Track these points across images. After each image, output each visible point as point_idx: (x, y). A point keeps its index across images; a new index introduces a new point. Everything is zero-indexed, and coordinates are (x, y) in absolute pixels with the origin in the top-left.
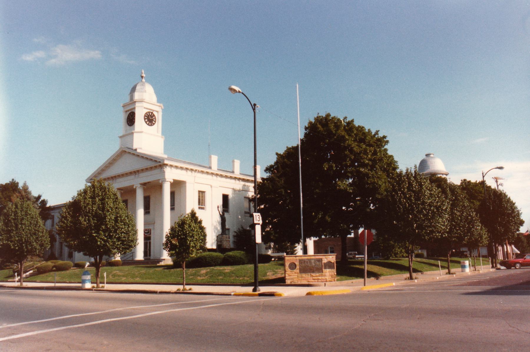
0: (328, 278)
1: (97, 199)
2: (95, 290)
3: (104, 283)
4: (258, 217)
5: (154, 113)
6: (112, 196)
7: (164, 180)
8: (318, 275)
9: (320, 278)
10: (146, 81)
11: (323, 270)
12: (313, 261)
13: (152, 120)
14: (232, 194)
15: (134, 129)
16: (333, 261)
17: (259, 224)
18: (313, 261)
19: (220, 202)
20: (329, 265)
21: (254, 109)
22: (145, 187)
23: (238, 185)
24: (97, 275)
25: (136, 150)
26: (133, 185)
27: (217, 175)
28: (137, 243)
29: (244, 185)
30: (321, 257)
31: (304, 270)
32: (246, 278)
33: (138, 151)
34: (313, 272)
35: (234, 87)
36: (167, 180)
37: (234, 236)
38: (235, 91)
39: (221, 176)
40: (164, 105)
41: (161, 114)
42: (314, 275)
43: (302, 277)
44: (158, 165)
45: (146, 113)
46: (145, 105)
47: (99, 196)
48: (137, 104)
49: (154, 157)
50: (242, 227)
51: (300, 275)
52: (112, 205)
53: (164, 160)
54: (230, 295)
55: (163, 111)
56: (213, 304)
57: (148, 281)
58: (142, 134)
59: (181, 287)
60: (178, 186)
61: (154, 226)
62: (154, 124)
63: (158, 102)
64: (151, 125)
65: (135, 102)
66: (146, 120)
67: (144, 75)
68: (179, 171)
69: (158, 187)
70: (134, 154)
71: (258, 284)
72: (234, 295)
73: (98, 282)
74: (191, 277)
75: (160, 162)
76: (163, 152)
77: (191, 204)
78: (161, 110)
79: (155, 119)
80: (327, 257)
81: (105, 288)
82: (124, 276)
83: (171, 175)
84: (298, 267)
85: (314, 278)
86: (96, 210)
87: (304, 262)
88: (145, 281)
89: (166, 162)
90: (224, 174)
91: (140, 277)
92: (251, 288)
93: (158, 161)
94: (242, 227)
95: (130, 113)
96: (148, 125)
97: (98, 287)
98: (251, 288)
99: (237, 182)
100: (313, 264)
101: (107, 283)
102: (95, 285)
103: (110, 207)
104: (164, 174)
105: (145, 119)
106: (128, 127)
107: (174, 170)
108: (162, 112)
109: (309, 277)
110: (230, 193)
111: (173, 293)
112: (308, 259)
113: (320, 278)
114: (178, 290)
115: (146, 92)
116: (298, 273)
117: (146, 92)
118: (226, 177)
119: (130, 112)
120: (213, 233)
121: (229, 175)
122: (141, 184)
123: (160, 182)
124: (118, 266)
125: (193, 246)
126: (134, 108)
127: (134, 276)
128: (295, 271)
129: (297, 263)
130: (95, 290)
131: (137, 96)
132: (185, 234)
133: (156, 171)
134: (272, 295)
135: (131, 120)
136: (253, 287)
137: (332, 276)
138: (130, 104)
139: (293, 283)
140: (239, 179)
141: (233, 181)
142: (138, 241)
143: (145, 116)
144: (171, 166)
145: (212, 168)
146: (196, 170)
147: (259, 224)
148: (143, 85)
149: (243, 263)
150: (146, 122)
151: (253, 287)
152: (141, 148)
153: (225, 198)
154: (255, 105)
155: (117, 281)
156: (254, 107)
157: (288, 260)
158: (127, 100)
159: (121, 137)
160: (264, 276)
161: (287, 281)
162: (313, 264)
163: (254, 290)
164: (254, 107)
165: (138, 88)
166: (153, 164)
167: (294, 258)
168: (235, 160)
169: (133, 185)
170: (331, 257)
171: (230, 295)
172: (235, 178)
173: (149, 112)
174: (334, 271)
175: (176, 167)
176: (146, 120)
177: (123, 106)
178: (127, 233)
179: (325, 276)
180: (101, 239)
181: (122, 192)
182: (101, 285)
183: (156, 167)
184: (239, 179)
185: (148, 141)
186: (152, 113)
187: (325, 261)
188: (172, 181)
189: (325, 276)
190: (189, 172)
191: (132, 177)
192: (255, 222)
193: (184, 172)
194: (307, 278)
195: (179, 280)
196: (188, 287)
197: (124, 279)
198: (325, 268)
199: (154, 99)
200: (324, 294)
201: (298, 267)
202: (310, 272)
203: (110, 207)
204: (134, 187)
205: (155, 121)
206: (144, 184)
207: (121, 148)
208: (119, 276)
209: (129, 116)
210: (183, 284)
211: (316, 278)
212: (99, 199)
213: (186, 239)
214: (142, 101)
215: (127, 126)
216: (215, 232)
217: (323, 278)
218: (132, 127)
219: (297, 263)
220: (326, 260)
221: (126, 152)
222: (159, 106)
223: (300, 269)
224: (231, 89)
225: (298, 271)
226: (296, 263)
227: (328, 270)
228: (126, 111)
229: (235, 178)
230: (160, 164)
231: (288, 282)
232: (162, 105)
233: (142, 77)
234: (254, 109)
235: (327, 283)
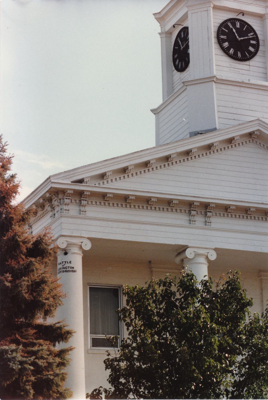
45: (224, 24)
62: (253, 55)
96: (234, 57)
105: (220, 42)
150: (226, 51)
173: (233, 21)
228: (169, 33)
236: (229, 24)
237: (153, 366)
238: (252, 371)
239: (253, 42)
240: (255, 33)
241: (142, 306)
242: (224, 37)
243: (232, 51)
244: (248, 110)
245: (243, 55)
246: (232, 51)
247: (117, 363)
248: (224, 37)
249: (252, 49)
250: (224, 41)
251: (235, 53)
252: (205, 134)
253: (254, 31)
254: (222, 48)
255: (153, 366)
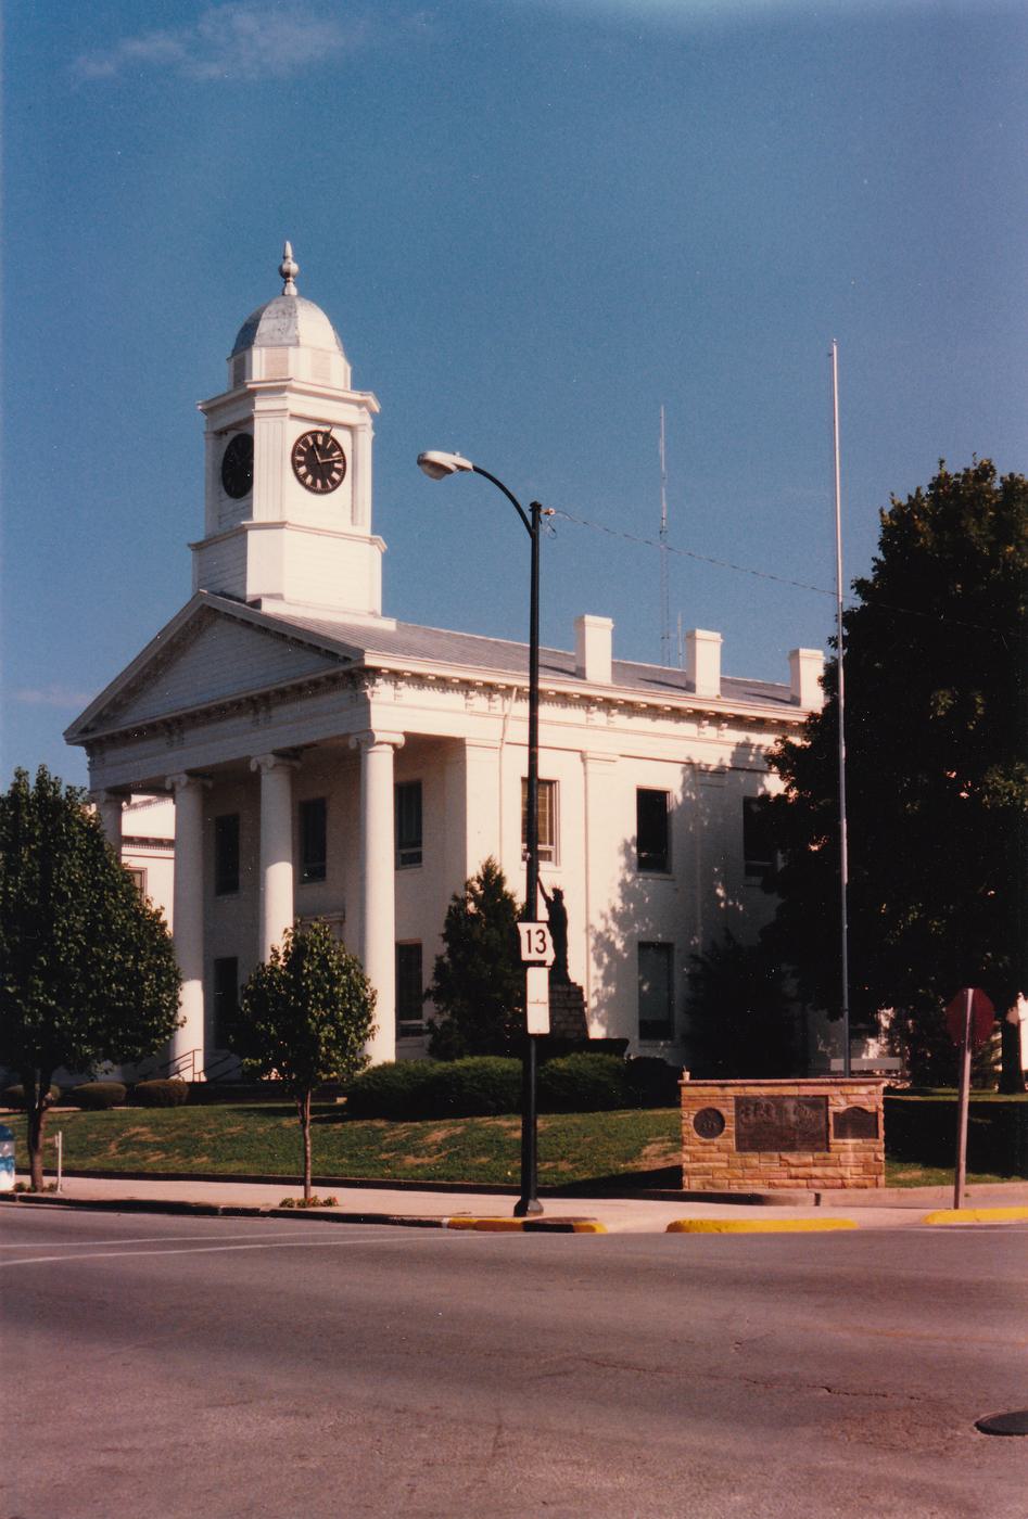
0: (850, 1172)
1: (25, 852)
2: (23, 1199)
3: (54, 1173)
4: (536, 939)
5: (337, 434)
6: (81, 841)
7: (367, 739)
8: (809, 1159)
9: (817, 1171)
10: (301, 294)
11: (832, 1140)
12: (790, 1105)
13: (330, 467)
14: (685, 787)
15: (249, 514)
16: (870, 1108)
17: (541, 964)
18: (790, 1105)
19: (626, 825)
20: (856, 1123)
21: (533, 531)
22: (297, 764)
23: (716, 748)
24: (33, 1146)
25: (257, 604)
26: (249, 758)
27: (608, 704)
28: (180, 1019)
29: (745, 747)
30: (823, 1090)
31: (750, 1141)
32: (564, 1166)
33: (268, 608)
34: (792, 1148)
35: (436, 456)
36: (378, 737)
37: (693, 978)
38: (441, 470)
39: (630, 708)
40: (379, 398)
41: (366, 438)
42: (792, 1158)
43: (745, 1166)
44: (333, 669)
45: (302, 439)
46: (295, 403)
47: (32, 839)
48: (261, 404)
49: (326, 639)
50: (729, 938)
51: (737, 1158)
52: (78, 874)
53: (361, 653)
54: (438, 1225)
55: (378, 422)
56: (130, 1237)
57: (233, 1167)
58: (285, 532)
59: (295, 1193)
60: (430, 766)
61: (341, 930)
62: (336, 484)
63: (357, 384)
64: (325, 491)
65: (253, 392)
66: (303, 470)
67: (293, 267)
68: (431, 696)
69: (346, 761)
70: (248, 624)
71: (533, 1193)
72: (451, 1226)
73: (39, 1167)
74: (384, 1156)
75: (346, 659)
76: (378, 608)
77: (489, 835)
78: (368, 421)
79: (344, 462)
80: (848, 1090)
81: (59, 1194)
82: (159, 1147)
83: (395, 714)
84: (730, 1127)
85: (793, 1171)
86: (20, 895)
87: (757, 1105)
88: (221, 1168)
89: (370, 660)
90: (641, 698)
91: (215, 1154)
92: (513, 1200)
93: (342, 654)
94: (729, 938)
95: (235, 441)
96: (311, 488)
97: (34, 1188)
98: (513, 1200)
99: (710, 731)
100: (793, 1118)
101: (66, 1173)
102: (26, 1180)
103: (70, 883)
104: (368, 712)
105: (296, 465)
106: (229, 503)
107: (409, 693)
108: (375, 427)
109: (776, 1165)
110: (671, 781)
111: (264, 1214)
112: (770, 1097)
113: (817, 1171)
114: (283, 1204)
115: (297, 344)
116: (728, 1151)
117: (297, 344)
118: (654, 712)
119: (232, 435)
120: (593, 965)
121: (666, 700)
122: (279, 754)
123: (352, 745)
124: (171, 1105)
125: (328, 1040)
126: (250, 420)
127: (191, 1147)
128: (717, 1140)
129: (729, 1112)
130: (23, 1199)
131: (261, 364)
132: (303, 995)
133: (338, 697)
134: (564, 1226)
135: (235, 470)
136: (517, 1199)
137: (865, 1165)
138: (233, 401)
139: (709, 1189)
140: (718, 719)
141: (688, 728)
142: (182, 1012)
143: (296, 451)
144: (395, 676)
145: (589, 673)
146: (509, 688)
147: (541, 964)
148: (289, 313)
149: (609, 1105)
150: (301, 479)
151: (517, 1199)
152: (279, 597)
153: (651, 804)
154: (535, 507)
155: (127, 1168)
156: (533, 520)
157: (691, 1098)
158: (221, 384)
159: (198, 547)
160: (626, 1160)
161: (685, 1179)
162: (793, 1118)
163: (520, 1210)
164: (533, 520)
165: (264, 327)
166: (325, 670)
167: (717, 1091)
168: (700, 633)
169: (249, 758)
170: (863, 1090)
171: (438, 1225)
172: (698, 716)
173: (314, 434)
174: (880, 1144)
175: (419, 680)
176: (303, 470)
177: (207, 411)
178: (134, 980)
179: (838, 1164)
180: (37, 1004)
181: (210, 784)
182: (47, 1181)
183: (333, 680)
184: (718, 719)
185: (315, 561)
186: (327, 435)
187: (839, 1105)
188: (400, 740)
189: (838, 1164)
190: (479, 701)
191: (242, 722)
192: (526, 956)
193: (455, 699)
194: (764, 1168)
195: (291, 1169)
196: (321, 1193)
197: (155, 1159)
198: (840, 1134)
199: (338, 371)
200: (724, 1231)
201: (730, 1127)
202: (777, 1149)
203: (70, 883)
204: (253, 768)
205: (342, 473)
206: (289, 755)
207: (197, 596)
208: (144, 1145)
209: (228, 454)
210: (302, 1182)
211: (801, 1171)
212: (32, 852)
213: (303, 1013)
214: (282, 389)
215: (225, 495)
216: (599, 961)
217: (830, 1171)
218: (241, 503)
219: (729, 1112)
220: (842, 1101)
221: (221, 612)
222: (360, 404)
223: (738, 1134)
224: (422, 462)
225: (732, 1142)
226: (724, 1112)
227: (850, 1141)
228: (221, 433)
229: (698, 716)
230: (346, 667)
231: (692, 1184)
232: (370, 398)
233: (286, 275)
234: (533, 531)
235: (825, 1194)
236: (309, 438)
237: (741, 909)
238: (381, 1130)
239: (337, 465)
240: (342, 454)
241: (86, 896)
242: (301, 458)
243: (309, 479)
244: (504, 730)
245: (324, 485)
246: (309, 479)
247: (24, 1007)
248: (301, 458)
249: (335, 476)
250: (300, 464)
251: (314, 483)
252: (305, 640)
253: (341, 450)
254: (307, 487)
255: (741, 909)
